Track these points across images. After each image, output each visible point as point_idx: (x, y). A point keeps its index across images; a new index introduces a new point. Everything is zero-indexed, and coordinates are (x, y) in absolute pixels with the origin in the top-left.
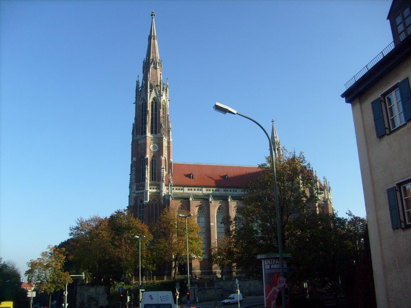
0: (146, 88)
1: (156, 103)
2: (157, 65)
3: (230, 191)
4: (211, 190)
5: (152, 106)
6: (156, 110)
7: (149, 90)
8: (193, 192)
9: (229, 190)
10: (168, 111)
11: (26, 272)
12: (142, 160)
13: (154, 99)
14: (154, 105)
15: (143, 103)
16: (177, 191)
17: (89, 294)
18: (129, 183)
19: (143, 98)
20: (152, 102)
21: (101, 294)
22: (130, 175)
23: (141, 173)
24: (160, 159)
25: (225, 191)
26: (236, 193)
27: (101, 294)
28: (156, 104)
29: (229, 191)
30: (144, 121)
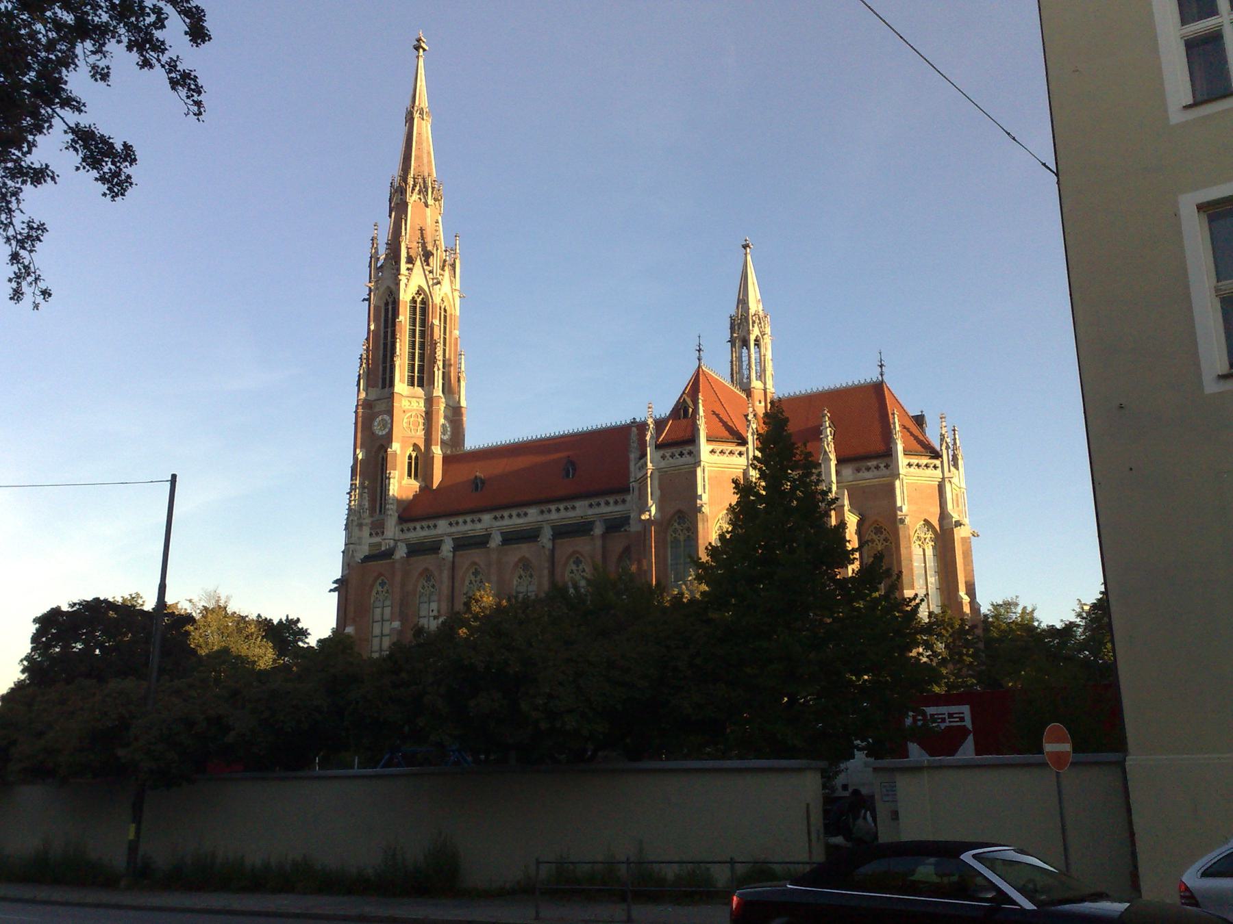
0: (398, 262)
1: (424, 302)
2: (427, 195)
3: (465, 522)
4: (882, 466)
5: (413, 309)
6: (424, 322)
7: (404, 266)
8: (604, 509)
9: (553, 507)
10: (457, 326)
11: (270, 620)
12: (381, 456)
13: (420, 291)
14: (417, 354)
16: (611, 508)
20: (414, 301)
24: (429, 454)
25: (542, 512)
26: (571, 514)
28: (422, 308)
29: (603, 504)
30: (389, 330)
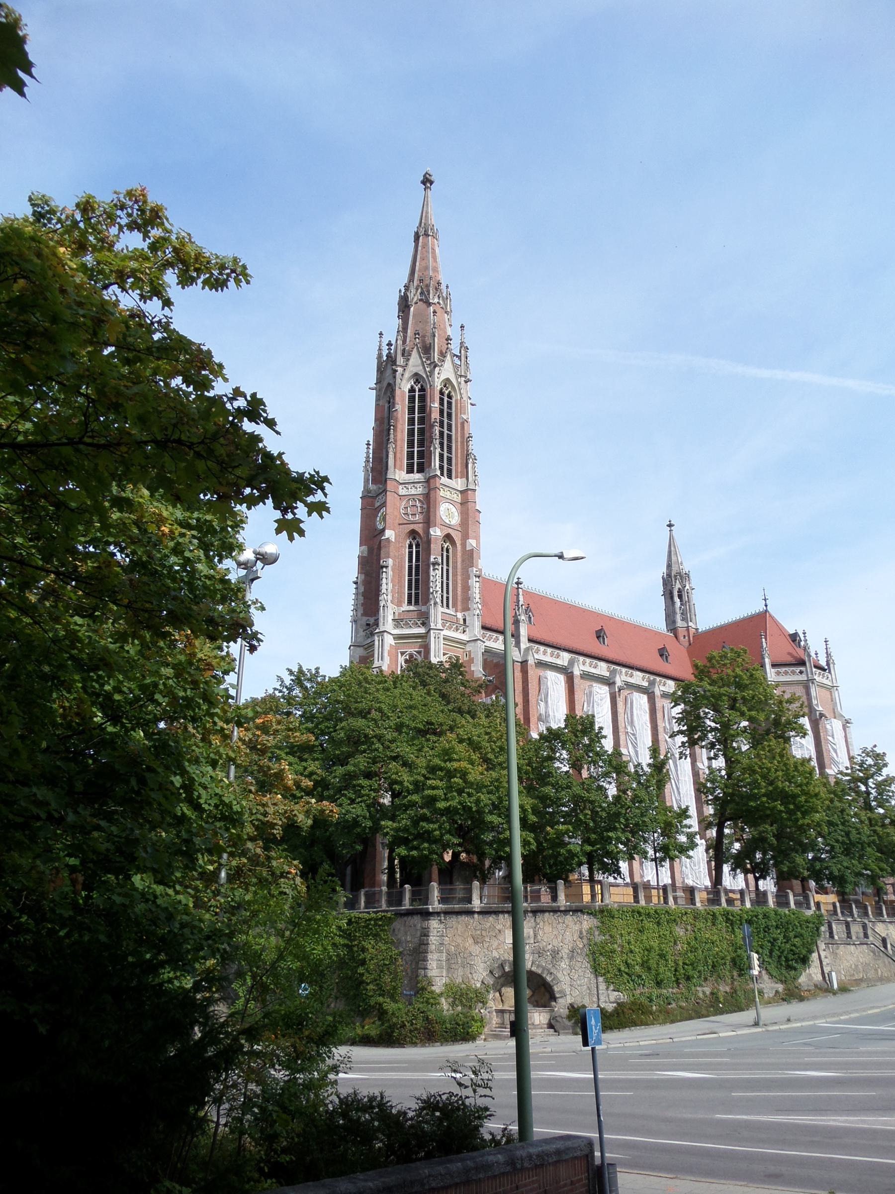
15: (412, 387)
17: (495, 954)
18: (352, 608)
19: (416, 374)
21: (565, 952)
22: (355, 586)
23: (407, 578)
27: (565, 952)
